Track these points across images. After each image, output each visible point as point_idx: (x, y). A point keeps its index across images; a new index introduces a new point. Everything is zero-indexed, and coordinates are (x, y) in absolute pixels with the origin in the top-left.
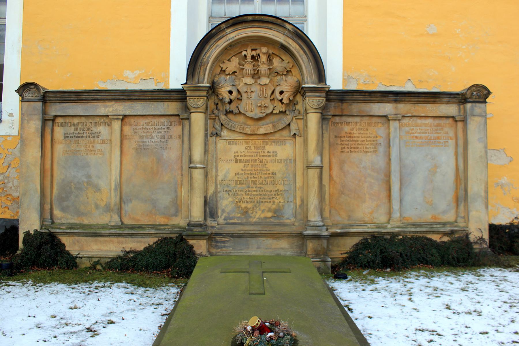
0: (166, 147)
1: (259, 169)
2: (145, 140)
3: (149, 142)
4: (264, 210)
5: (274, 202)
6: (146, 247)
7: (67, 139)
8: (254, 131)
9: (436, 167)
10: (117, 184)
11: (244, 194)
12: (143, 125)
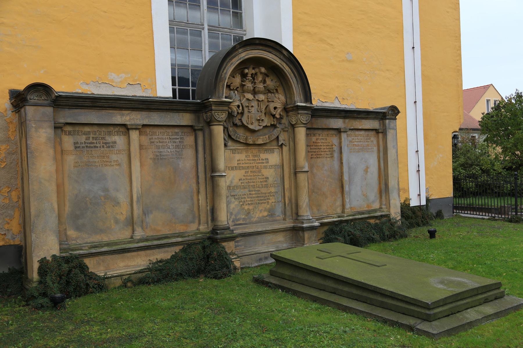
0: (181, 157)
1: (256, 174)
2: (161, 150)
3: (166, 152)
4: (261, 210)
5: (268, 202)
6: (173, 255)
7: (78, 149)
8: (254, 142)
9: (367, 168)
10: (139, 196)
11: (247, 198)
12: (159, 135)
